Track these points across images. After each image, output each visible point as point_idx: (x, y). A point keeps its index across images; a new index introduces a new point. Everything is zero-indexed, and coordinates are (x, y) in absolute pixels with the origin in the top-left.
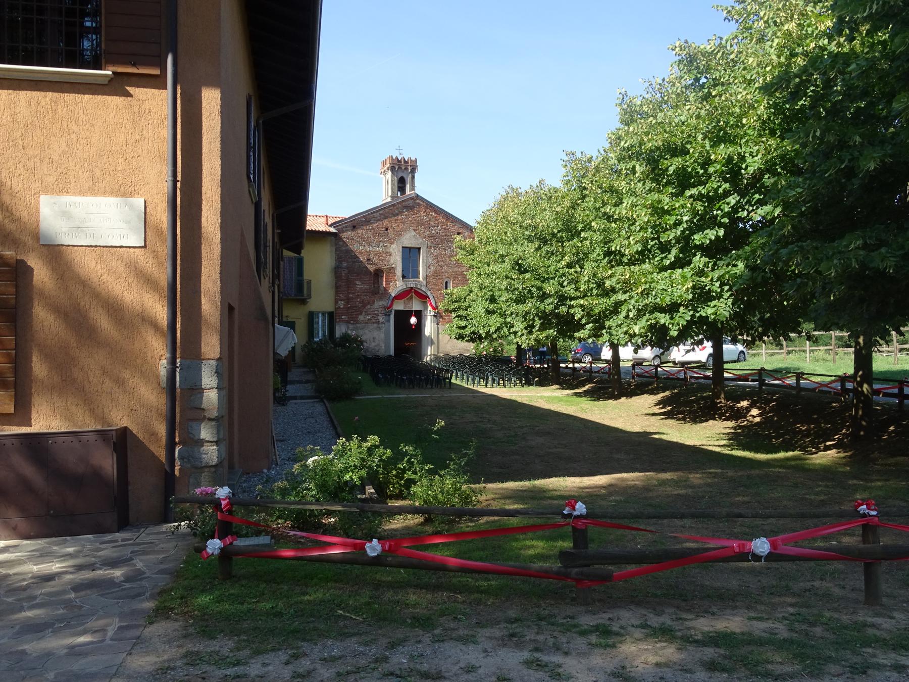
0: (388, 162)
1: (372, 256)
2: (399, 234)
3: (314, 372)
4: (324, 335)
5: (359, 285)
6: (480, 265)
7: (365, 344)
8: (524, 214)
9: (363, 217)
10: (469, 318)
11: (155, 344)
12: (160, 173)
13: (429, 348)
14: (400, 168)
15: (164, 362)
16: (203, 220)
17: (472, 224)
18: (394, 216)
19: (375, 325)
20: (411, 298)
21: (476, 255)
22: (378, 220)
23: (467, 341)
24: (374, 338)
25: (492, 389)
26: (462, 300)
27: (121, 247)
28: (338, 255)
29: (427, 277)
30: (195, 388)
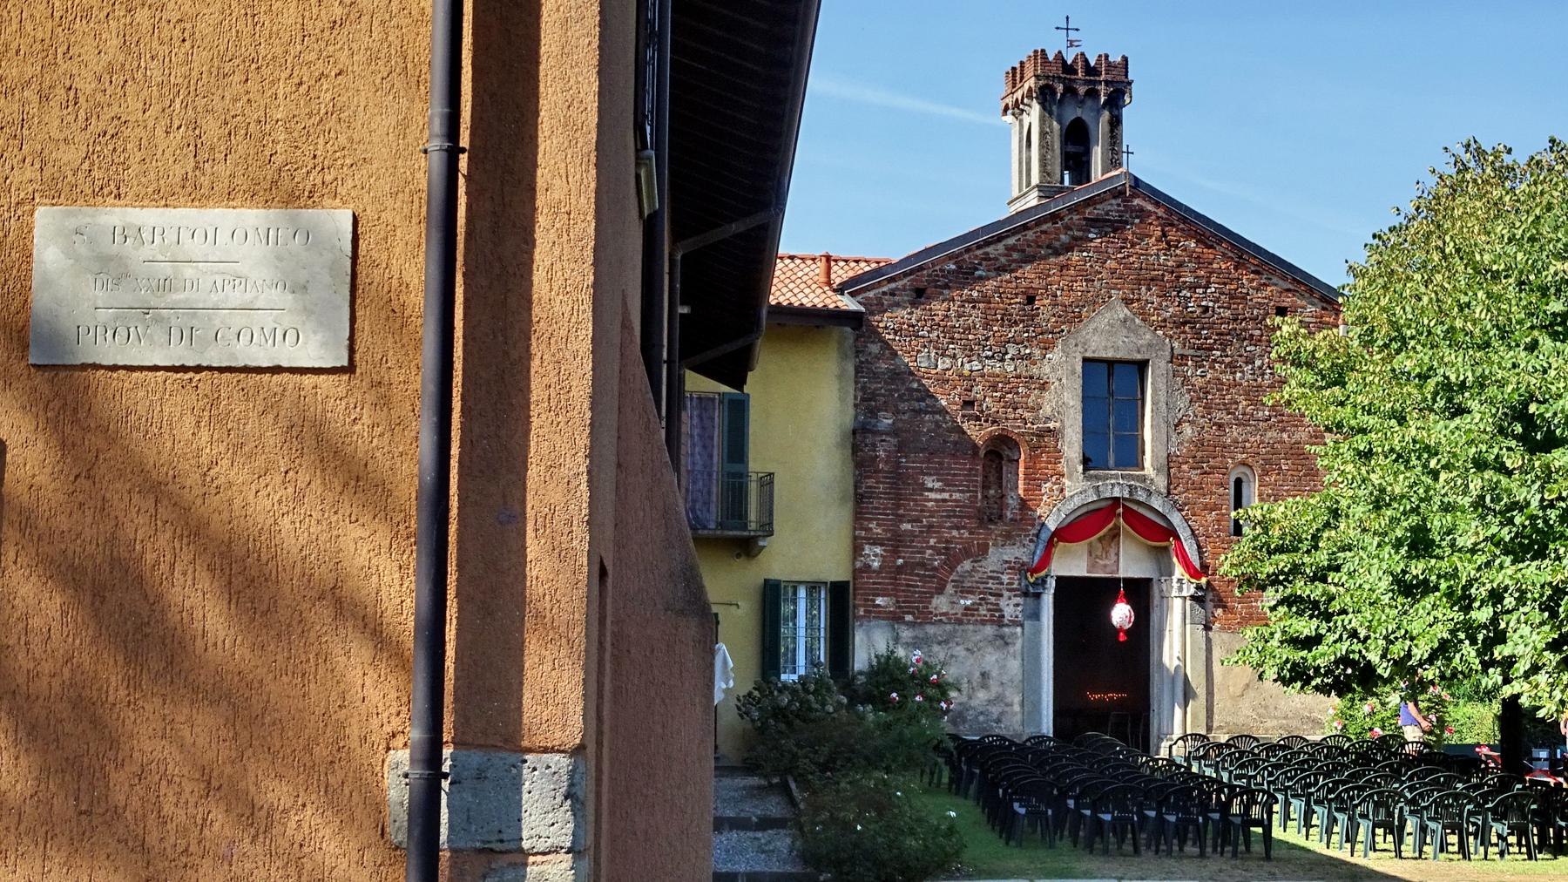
0: (1029, 72)
1: (978, 391)
2: (1072, 316)
3: (784, 789)
4: (813, 662)
5: (935, 492)
6: (1372, 421)
7: (953, 694)
8: (1532, 239)
9: (950, 257)
10: (1335, 606)
11: (374, 696)
12: (404, 124)
13: (1178, 712)
14: (1070, 91)
15: (402, 756)
16: (539, 277)
17: (1332, 275)
18: (1057, 253)
19: (989, 630)
20: (1115, 535)
21: (1351, 387)
22: (1001, 270)
23: (1317, 688)
24: (984, 675)
25: (1421, 864)
26: (1304, 546)
27: (277, 370)
28: (863, 389)
29: (1169, 464)
30: (497, 846)
